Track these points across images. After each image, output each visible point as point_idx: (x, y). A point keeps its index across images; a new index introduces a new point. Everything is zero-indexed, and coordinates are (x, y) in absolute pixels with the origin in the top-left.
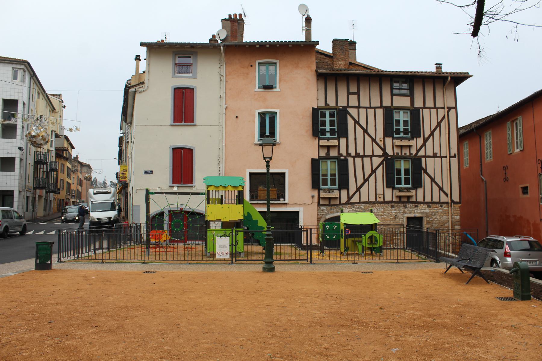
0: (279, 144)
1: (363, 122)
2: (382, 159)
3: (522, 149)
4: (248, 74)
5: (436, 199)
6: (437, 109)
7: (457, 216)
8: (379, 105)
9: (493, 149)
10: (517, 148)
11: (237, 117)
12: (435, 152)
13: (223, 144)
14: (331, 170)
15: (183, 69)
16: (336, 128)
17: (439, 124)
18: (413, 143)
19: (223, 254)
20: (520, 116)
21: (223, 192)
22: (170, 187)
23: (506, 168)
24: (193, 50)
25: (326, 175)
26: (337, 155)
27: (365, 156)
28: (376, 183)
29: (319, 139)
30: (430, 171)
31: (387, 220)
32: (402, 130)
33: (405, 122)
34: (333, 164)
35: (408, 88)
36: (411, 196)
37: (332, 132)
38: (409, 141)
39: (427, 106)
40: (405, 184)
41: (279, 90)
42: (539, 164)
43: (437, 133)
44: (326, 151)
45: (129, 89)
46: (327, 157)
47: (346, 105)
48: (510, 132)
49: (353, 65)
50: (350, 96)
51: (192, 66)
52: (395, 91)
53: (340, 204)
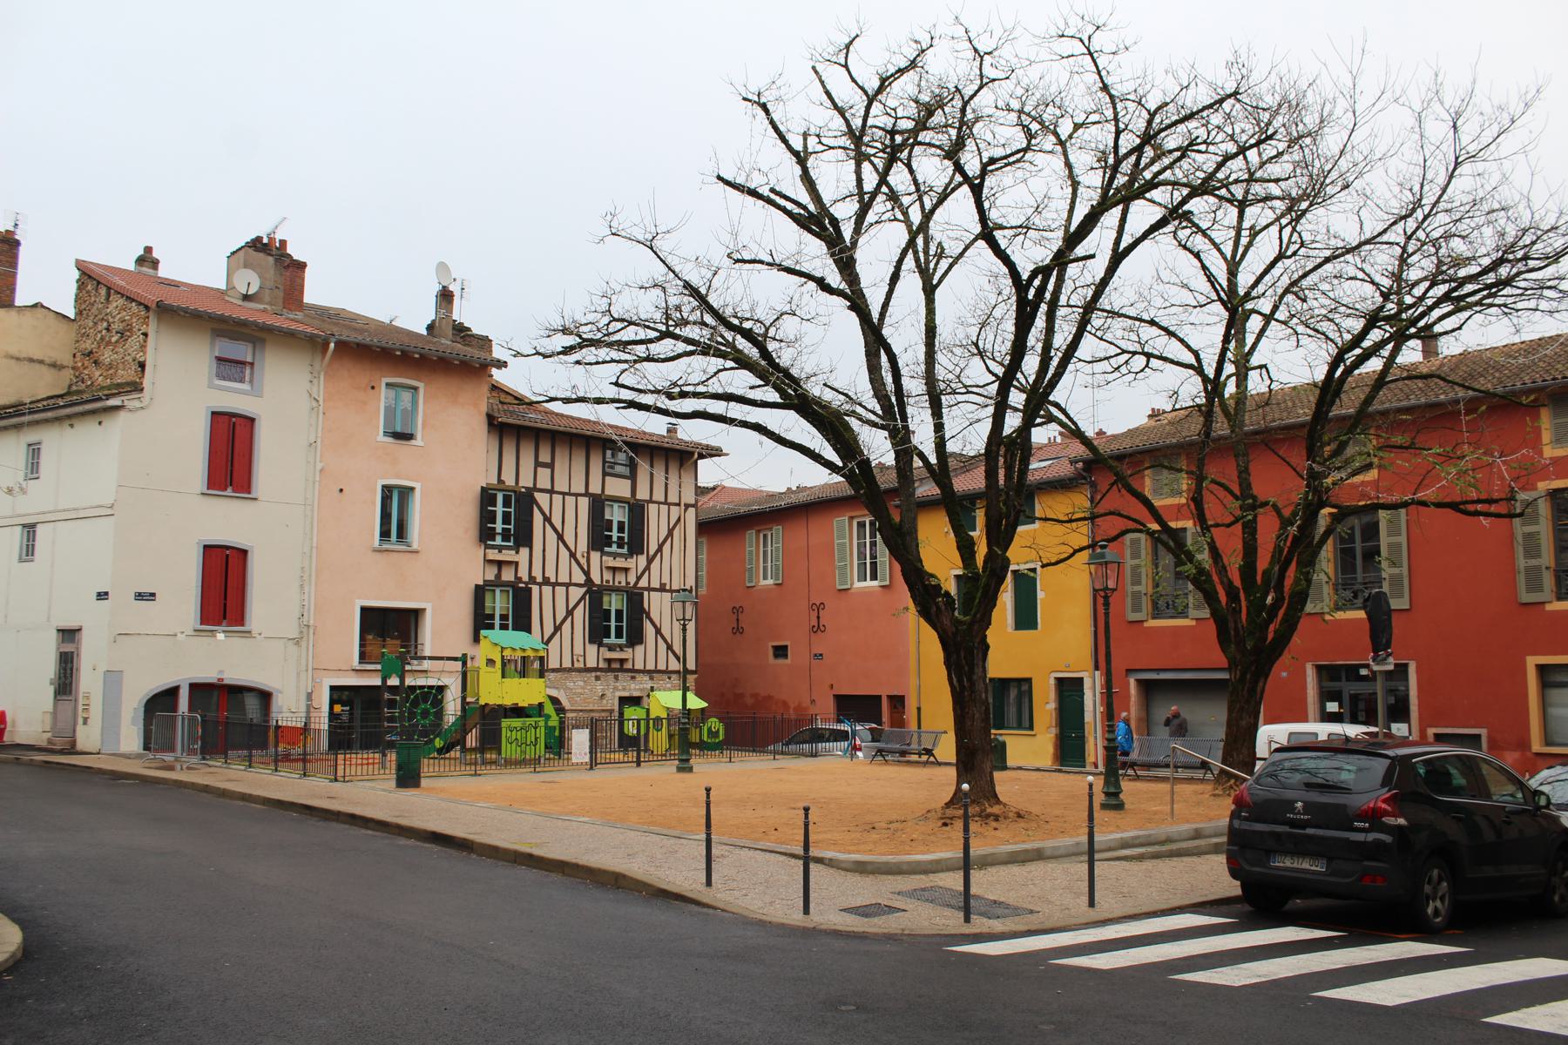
1: (557, 521)
2: (584, 589)
3: (780, 582)
5: (662, 666)
6: (669, 504)
8: (583, 492)
9: (708, 572)
10: (765, 578)
11: (341, 490)
15: (234, 370)
16: (512, 527)
17: (670, 533)
18: (630, 563)
22: (195, 630)
27: (557, 584)
28: (572, 633)
30: (655, 615)
31: (589, 703)
32: (499, 530)
33: (621, 525)
36: (627, 660)
39: (654, 499)
46: (497, 583)
50: (539, 469)
52: (607, 470)
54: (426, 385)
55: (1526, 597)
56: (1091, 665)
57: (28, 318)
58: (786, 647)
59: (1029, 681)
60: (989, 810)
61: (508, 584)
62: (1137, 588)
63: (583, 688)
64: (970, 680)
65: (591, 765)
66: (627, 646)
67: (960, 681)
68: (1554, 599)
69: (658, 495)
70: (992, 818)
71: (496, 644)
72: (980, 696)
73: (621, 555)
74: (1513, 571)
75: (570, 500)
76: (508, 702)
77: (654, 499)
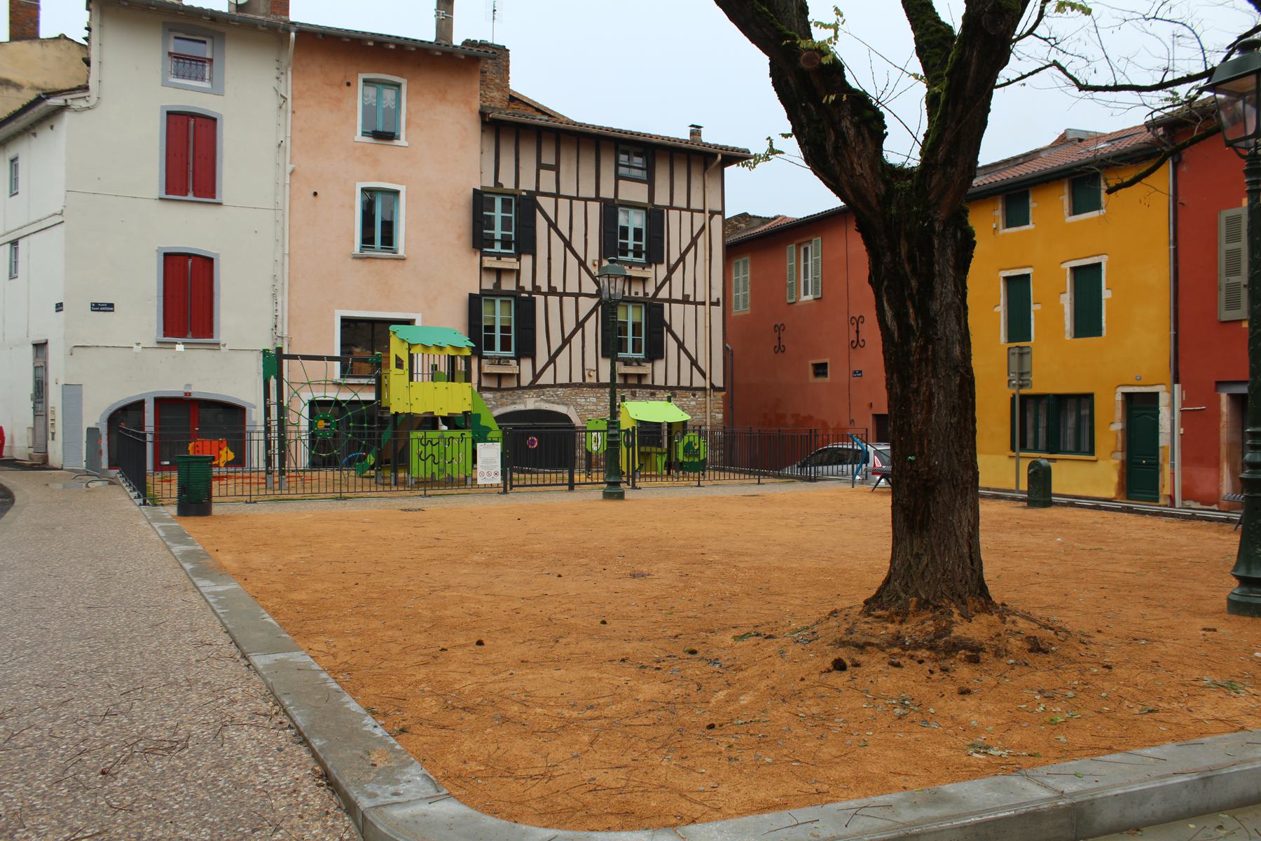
0: (404, 259)
1: (563, 226)
2: (595, 301)
3: (819, 296)
4: (340, 101)
5: (685, 382)
6: (693, 211)
7: (718, 413)
8: (594, 196)
9: (751, 291)
11: (315, 194)
12: (685, 293)
13: (284, 251)
14: (501, 319)
16: (512, 233)
17: (694, 241)
18: (649, 273)
19: (489, 475)
20: (816, 237)
21: (437, 357)
22: (158, 342)
23: (782, 328)
24: (213, 27)
25: (491, 328)
26: (515, 289)
28: (583, 347)
29: (483, 254)
30: (676, 328)
32: (631, 247)
33: (638, 233)
34: (638, 310)
35: (645, 166)
36: (645, 375)
37: (506, 243)
38: (644, 269)
40: (502, 349)
41: (406, 144)
42: (853, 324)
43: (690, 257)
44: (495, 281)
45: (48, 98)
46: (496, 293)
47: (533, 189)
48: (794, 263)
49: (516, 102)
51: (211, 66)
52: (622, 171)
53: (519, 387)
54: (409, 81)
56: (1169, 377)
57: (51, 50)
58: (826, 364)
59: (1089, 397)
60: (963, 630)
61: (508, 294)
62: (1234, 279)
64: (923, 311)
65: (505, 488)
66: (644, 361)
67: (900, 316)
69: (680, 201)
70: (962, 654)
71: (403, 341)
72: (948, 352)
73: (638, 264)
76: (419, 409)
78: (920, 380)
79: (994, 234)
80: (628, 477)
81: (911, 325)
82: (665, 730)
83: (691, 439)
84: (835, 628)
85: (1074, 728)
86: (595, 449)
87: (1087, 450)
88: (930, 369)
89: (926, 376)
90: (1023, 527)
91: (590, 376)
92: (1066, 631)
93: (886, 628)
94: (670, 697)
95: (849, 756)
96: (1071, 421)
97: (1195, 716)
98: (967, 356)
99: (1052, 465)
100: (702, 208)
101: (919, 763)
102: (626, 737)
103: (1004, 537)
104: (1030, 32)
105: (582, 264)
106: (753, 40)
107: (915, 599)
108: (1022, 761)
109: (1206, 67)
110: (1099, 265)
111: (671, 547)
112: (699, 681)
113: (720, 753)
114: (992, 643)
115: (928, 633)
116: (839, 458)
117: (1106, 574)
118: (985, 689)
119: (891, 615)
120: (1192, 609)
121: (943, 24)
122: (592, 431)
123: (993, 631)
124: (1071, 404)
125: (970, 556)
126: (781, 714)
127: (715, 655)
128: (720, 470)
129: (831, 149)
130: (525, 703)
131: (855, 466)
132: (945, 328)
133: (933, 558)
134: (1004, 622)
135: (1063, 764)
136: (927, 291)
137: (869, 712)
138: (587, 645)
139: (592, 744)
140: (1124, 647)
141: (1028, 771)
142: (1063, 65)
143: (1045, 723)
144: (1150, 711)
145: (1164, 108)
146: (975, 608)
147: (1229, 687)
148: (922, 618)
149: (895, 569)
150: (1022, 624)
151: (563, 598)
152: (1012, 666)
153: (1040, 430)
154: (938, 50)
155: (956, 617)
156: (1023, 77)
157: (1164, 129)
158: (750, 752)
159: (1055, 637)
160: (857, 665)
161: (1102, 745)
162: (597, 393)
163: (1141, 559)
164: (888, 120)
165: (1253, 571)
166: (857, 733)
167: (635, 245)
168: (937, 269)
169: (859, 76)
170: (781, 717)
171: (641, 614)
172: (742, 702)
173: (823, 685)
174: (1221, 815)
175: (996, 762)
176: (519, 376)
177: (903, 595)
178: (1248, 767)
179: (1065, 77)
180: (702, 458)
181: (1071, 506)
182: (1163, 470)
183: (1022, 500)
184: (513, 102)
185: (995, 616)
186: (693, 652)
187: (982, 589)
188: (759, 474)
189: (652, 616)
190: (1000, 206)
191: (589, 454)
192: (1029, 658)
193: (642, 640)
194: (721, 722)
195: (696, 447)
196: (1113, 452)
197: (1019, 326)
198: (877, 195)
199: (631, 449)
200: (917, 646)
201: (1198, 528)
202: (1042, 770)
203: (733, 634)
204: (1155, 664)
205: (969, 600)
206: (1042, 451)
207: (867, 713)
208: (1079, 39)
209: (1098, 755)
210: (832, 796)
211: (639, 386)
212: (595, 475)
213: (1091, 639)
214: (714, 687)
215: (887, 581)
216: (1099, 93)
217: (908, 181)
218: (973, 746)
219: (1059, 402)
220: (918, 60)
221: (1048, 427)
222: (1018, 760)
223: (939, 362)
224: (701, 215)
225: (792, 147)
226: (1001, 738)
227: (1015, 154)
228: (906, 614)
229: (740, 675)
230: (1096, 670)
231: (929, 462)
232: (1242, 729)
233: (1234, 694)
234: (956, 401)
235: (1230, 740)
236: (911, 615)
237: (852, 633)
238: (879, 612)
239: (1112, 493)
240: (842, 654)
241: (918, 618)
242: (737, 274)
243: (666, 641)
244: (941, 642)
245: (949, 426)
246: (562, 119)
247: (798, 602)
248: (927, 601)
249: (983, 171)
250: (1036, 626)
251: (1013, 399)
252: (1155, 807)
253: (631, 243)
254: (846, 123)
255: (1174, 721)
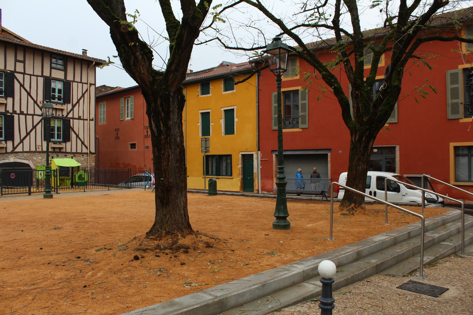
1: (27, 86)
3: (133, 118)
5: (79, 151)
6: (83, 83)
9: (106, 115)
12: (79, 116)
16: (3, 88)
17: (83, 95)
18: (64, 107)
23: (118, 130)
28: (36, 136)
30: (76, 129)
32: (57, 96)
33: (60, 91)
34: (59, 122)
35: (63, 64)
36: (62, 148)
38: (62, 105)
39: (76, 80)
43: (81, 101)
47: (13, 70)
48: (123, 105)
52: (53, 65)
53: (6, 153)
55: (451, 116)
59: (230, 156)
60: (182, 241)
63: (41, 160)
64: (166, 125)
66: (62, 142)
67: (158, 126)
68: (463, 117)
69: (78, 79)
70: (182, 250)
72: (175, 140)
73: (60, 103)
74: (446, 105)
75: (34, 78)
77: (76, 80)
78: (165, 150)
79: (197, 97)
80: (55, 189)
81: (162, 130)
82: (66, 290)
83: (81, 173)
84: (135, 244)
85: (221, 273)
86: (40, 178)
87: (230, 174)
88: (168, 146)
89: (167, 148)
90: (207, 203)
91: (39, 148)
92: (219, 239)
93: (154, 243)
94: (68, 277)
95: (140, 292)
96: (224, 165)
97: (261, 265)
98: (182, 141)
99: (217, 180)
100: (87, 82)
101: (166, 292)
102: (49, 295)
103: (199, 207)
104: (210, 26)
105: (35, 102)
106: (103, 19)
107: (164, 231)
108: (202, 287)
109: (266, 45)
110: (234, 109)
111: (72, 216)
112: (81, 269)
113: (89, 296)
114: (193, 245)
115: (169, 244)
116: (140, 179)
117: (234, 218)
118: (190, 262)
119: (156, 238)
120: (262, 228)
121: (177, 20)
122: (39, 171)
123: (193, 241)
124: (224, 159)
125: (184, 214)
126: (114, 279)
127: (88, 258)
128: (93, 185)
129: (132, 63)
130: (3, 286)
131: (146, 182)
132: (174, 131)
133: (171, 216)
134: (197, 238)
135: (217, 286)
136: (167, 117)
137: (148, 275)
138: (34, 259)
139: (33, 300)
140: (239, 243)
141: (205, 290)
142: (220, 39)
143: (211, 272)
144: (246, 265)
145: (253, 57)
146: (187, 233)
147: (272, 254)
148: (167, 238)
149: (157, 220)
150: (204, 238)
151: (23, 240)
152: (200, 253)
153: (214, 168)
154: (174, 30)
155: (180, 237)
156: (207, 42)
157: (255, 64)
158: (101, 295)
159: (215, 241)
160: (143, 257)
161: (230, 278)
162: (41, 155)
163: (246, 212)
164: (154, 53)
165: (280, 214)
166: (143, 283)
167: (58, 96)
168: (171, 109)
169: (143, 36)
170: (113, 280)
171: (58, 244)
172: (98, 276)
173: (130, 266)
174: (268, 297)
175: (194, 288)
176: (6, 148)
177: (160, 230)
178: (276, 279)
179: (221, 43)
180: (85, 181)
181: (224, 195)
182: (255, 181)
183: (207, 193)
184: (3, 32)
185: (194, 236)
186: (79, 258)
187: (189, 226)
188: (109, 186)
189: (62, 245)
190: (200, 87)
191: (38, 180)
192: (206, 250)
193: (58, 254)
194: (89, 284)
195: (83, 176)
196: (238, 175)
197: (206, 130)
198: (149, 81)
199: (56, 178)
200: (165, 248)
201: (265, 200)
202: (209, 289)
203: (95, 249)
204: (249, 248)
205: (185, 230)
206: (214, 175)
207: (147, 275)
208: (226, 31)
209: (229, 282)
210: (133, 308)
211: (59, 152)
212: (40, 189)
213: (228, 241)
214: (87, 271)
215: (154, 225)
216: (232, 49)
217: (161, 77)
218: (186, 283)
219: (220, 158)
220: (167, 32)
221: (216, 167)
222: (202, 286)
223: (172, 143)
224: (86, 85)
225: (118, 61)
226: (196, 280)
227: (205, 69)
228: (162, 237)
229: (98, 265)
230: (229, 252)
231: (169, 180)
232: (275, 267)
233: (273, 256)
234: (178, 158)
235: (272, 271)
236: (163, 237)
237: (141, 246)
238: (152, 237)
239: (238, 190)
240: (138, 254)
241: (166, 238)
242: (101, 109)
243: (68, 254)
244: (174, 246)
245: (176, 167)
246: (27, 42)
247: (122, 235)
248: (169, 232)
249: (194, 74)
250: (209, 238)
251: (204, 157)
252: (247, 297)
253: (57, 95)
254: (138, 54)
255: (254, 267)
